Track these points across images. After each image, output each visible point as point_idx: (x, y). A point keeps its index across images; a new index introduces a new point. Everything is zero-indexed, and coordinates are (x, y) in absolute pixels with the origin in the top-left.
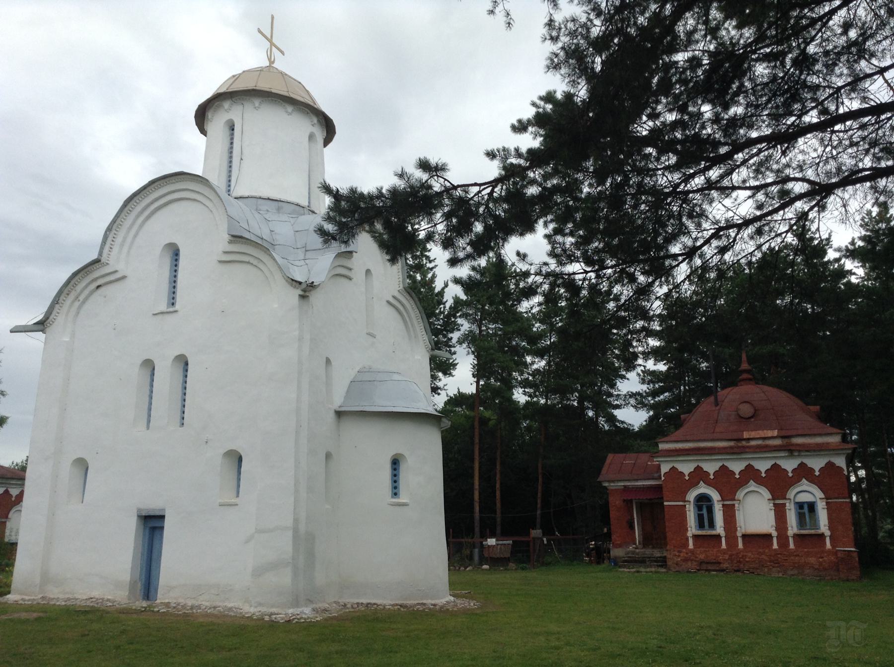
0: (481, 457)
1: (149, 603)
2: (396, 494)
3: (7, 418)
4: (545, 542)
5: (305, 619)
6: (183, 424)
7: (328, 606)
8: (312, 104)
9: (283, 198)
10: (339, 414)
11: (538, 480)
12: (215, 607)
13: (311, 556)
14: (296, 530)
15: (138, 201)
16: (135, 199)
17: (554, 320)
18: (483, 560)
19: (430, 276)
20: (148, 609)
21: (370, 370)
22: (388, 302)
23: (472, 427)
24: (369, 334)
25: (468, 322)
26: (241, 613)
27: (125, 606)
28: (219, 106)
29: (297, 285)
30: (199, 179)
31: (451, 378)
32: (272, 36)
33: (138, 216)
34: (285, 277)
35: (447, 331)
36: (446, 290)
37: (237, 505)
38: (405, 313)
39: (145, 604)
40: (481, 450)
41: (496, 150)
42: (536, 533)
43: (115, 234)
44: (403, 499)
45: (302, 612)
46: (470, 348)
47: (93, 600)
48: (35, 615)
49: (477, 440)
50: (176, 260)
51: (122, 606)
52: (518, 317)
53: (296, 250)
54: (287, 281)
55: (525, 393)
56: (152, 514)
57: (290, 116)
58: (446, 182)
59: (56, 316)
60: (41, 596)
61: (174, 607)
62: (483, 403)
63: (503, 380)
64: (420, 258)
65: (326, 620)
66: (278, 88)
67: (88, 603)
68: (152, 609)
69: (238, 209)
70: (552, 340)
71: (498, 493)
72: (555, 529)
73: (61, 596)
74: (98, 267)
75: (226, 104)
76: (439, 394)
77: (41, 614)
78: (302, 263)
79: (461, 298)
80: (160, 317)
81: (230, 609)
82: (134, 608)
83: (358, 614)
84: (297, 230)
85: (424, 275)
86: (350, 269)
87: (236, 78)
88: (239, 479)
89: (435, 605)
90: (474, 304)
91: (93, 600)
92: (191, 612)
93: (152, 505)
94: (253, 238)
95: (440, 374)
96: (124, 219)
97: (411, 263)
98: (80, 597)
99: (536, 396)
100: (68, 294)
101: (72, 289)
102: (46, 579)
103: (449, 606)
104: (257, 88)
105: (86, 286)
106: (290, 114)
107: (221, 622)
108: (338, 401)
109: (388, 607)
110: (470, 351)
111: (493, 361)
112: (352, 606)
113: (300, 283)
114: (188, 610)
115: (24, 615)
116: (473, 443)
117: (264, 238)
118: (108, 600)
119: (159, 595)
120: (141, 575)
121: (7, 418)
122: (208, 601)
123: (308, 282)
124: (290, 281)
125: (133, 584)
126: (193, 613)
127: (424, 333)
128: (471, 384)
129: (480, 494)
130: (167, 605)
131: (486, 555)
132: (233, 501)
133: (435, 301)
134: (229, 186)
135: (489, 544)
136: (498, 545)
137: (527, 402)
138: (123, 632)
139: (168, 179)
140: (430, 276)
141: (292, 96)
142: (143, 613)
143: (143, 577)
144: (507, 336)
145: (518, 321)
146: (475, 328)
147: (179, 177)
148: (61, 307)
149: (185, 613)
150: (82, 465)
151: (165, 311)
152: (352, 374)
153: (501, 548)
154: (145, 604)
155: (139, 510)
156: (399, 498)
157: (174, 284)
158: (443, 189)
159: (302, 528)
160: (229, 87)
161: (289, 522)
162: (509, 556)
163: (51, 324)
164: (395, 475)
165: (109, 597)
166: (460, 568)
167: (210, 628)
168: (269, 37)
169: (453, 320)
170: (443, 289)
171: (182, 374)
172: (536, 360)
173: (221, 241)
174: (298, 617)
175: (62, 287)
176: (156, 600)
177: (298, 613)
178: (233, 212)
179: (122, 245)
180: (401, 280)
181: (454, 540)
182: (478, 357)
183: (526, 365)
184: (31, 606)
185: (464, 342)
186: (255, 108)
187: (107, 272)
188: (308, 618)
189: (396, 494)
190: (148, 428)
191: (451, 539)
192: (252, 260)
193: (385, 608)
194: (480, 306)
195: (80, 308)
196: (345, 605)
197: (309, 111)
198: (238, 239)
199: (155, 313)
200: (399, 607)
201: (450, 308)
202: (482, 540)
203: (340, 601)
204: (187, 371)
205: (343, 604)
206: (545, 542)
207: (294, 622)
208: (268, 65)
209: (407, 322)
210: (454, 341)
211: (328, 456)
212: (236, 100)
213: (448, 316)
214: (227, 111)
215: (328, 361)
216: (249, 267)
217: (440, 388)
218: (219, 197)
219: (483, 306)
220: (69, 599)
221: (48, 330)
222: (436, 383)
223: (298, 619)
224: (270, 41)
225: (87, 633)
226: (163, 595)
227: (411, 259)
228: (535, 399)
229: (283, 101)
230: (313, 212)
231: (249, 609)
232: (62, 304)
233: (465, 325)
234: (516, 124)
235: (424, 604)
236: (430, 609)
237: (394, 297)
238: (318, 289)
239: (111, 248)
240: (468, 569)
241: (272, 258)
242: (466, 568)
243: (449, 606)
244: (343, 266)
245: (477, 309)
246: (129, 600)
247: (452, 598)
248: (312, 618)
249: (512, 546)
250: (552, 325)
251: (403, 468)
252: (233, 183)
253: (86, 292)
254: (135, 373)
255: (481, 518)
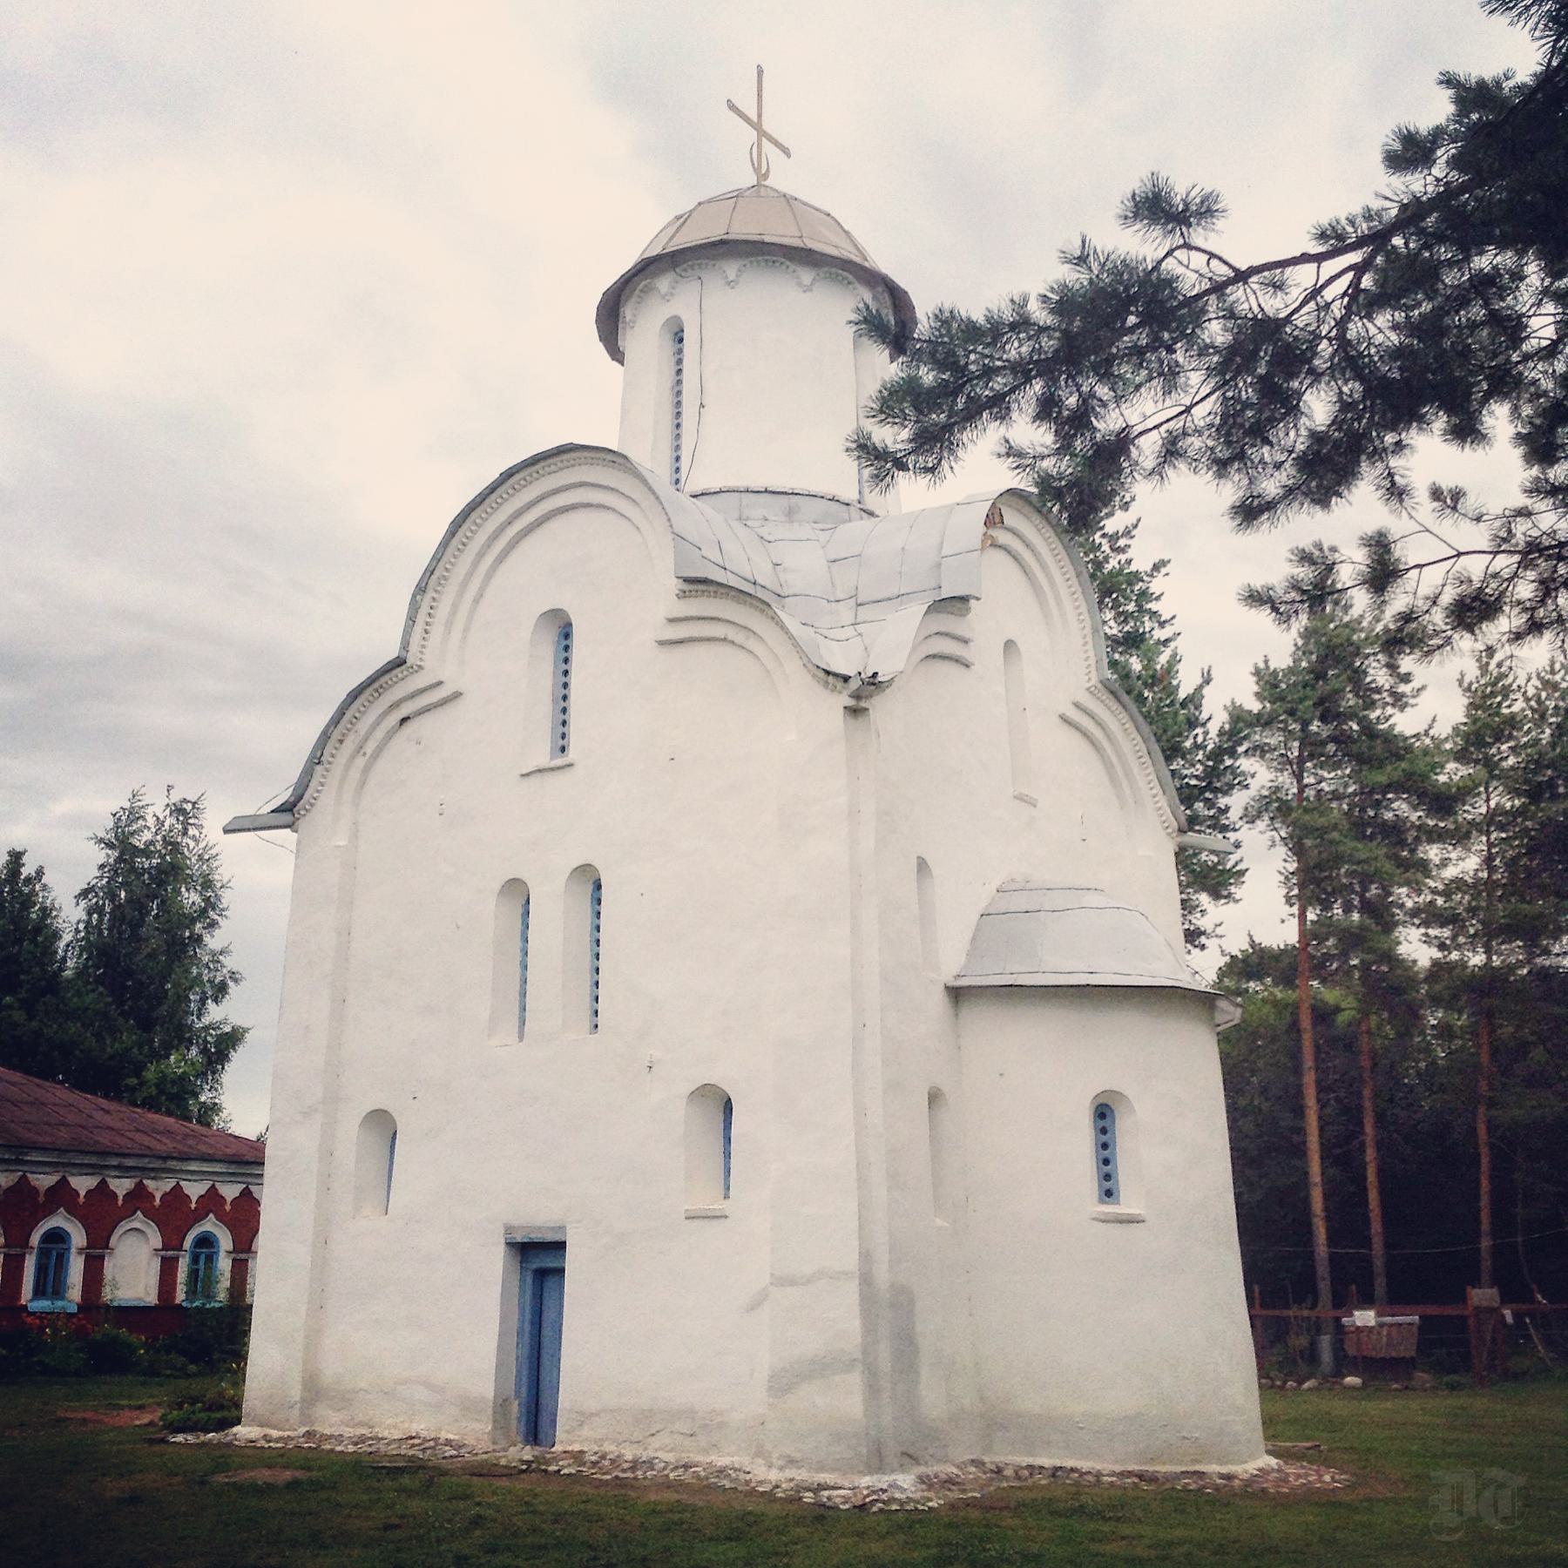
0: (1322, 1105)
1: (538, 1450)
2: (1109, 1193)
3: (246, 1030)
4: (1509, 1319)
5: (901, 1503)
6: (597, 1026)
7: (955, 1471)
8: (858, 260)
9: (799, 486)
10: (957, 994)
11: (1479, 1161)
12: (686, 1467)
13: (906, 1345)
14: (866, 1280)
15: (478, 521)
16: (474, 515)
17: (1494, 751)
18: (1344, 1364)
19: (1163, 659)
20: (534, 1465)
21: (1026, 888)
22: (1065, 719)
23: (1294, 1027)
24: (1019, 798)
25: (1269, 768)
26: (747, 1482)
27: (485, 1456)
28: (647, 290)
29: (840, 684)
30: (610, 457)
31: (1231, 904)
32: (760, 116)
33: (481, 555)
34: (809, 666)
35: (1216, 790)
36: (1205, 691)
37: (726, 1217)
38: (1106, 744)
39: (528, 1453)
40: (1321, 1088)
41: (1344, 222)
42: (1482, 1296)
43: (434, 599)
44: (1128, 1204)
45: (893, 1485)
46: (1275, 829)
47: (416, 1441)
48: (288, 1475)
49: (1308, 1062)
50: (567, 648)
51: (478, 1458)
52: (1396, 748)
53: (834, 604)
54: (814, 676)
55: (1427, 939)
56: (537, 1237)
57: (808, 294)
58: (1214, 262)
59: (318, 791)
60: (303, 1430)
61: (594, 1464)
62: (1319, 968)
63: (1367, 907)
64: (1136, 620)
65: (952, 1506)
66: (780, 231)
67: (404, 1450)
68: (543, 1467)
69: (700, 521)
70: (1493, 804)
71: (1373, 1196)
72: (1534, 1286)
73: (348, 1432)
74: (400, 675)
75: (664, 283)
76: (1203, 947)
77: (299, 1474)
78: (849, 632)
79: (1247, 707)
80: (533, 780)
81: (721, 1471)
82: (503, 1462)
83: (1032, 1495)
84: (832, 558)
85: (1149, 661)
86: (966, 642)
87: (682, 220)
88: (727, 1155)
89: (1229, 1477)
90: (1282, 721)
91: (416, 1441)
92: (629, 1475)
93: (538, 1218)
94: (733, 581)
95: (1204, 899)
96: (452, 564)
97: (1115, 631)
98: (386, 1434)
99: (1459, 947)
100: (341, 741)
101: (348, 730)
102: (314, 1391)
103: (1267, 1481)
104: (731, 237)
105: (377, 723)
106: (808, 289)
107: (701, 1504)
108: (952, 964)
109: (1110, 1479)
110: (1278, 839)
111: (1338, 860)
112: (1016, 1472)
113: (846, 679)
114: (624, 1471)
115: (263, 1476)
116: (1297, 1070)
117: (760, 581)
118: (448, 1443)
119: (560, 1434)
120: (518, 1384)
121: (246, 1030)
122: (671, 1451)
123: (863, 676)
124: (822, 674)
125: (501, 1405)
126: (635, 1478)
127: (1157, 790)
128: (1283, 921)
129: (1326, 1197)
130: (578, 1456)
131: (1351, 1351)
132: (719, 1206)
133: (1181, 718)
134: (678, 470)
135: (1359, 1324)
136: (1381, 1325)
137: (1435, 963)
138: (477, 1521)
139: (542, 464)
140: (1163, 659)
141: (811, 244)
142: (523, 1476)
143: (524, 1390)
144: (1372, 796)
145: (1400, 758)
146: (1286, 780)
147: (565, 457)
148: (327, 770)
149: (617, 1477)
150: (382, 1125)
151: (547, 766)
152: (982, 897)
153: (1389, 1335)
154: (528, 1453)
155: (509, 1229)
156: (1118, 1203)
157: (563, 704)
158: (1206, 285)
159: (882, 1275)
160: (667, 243)
161: (851, 1262)
162: (1413, 1354)
163: (307, 810)
164: (1105, 1146)
165: (451, 1436)
166: (1285, 1383)
167: (676, 1517)
168: (754, 117)
169: (1228, 762)
170: (1200, 688)
171: (589, 910)
172: (1453, 855)
173: (662, 596)
174: (884, 1497)
175: (328, 726)
176: (553, 1446)
177: (885, 1487)
178: (684, 525)
179: (449, 624)
180: (1092, 661)
181: (1264, 1312)
182: (1298, 850)
183: (1424, 867)
184: (282, 1453)
185: (1259, 816)
186: (729, 284)
187: (422, 686)
188: (910, 1500)
189: (1109, 1193)
190: (521, 1037)
191: (1258, 1311)
192: (731, 633)
193: (1098, 1481)
194: (1295, 726)
195: (367, 770)
196: (999, 1471)
197: (851, 277)
198: (701, 587)
199: (524, 772)
200: (1136, 1480)
201: (1221, 733)
202: (1338, 1313)
203: (986, 1459)
204: (599, 902)
205: (993, 1467)
206: (1509, 1319)
207: (875, 1509)
208: (755, 183)
209: (1112, 766)
210: (1234, 815)
211: (934, 1098)
212: (685, 270)
213: (1217, 754)
214: (666, 298)
215: (922, 865)
216: (728, 650)
217: (1203, 933)
218: (654, 493)
219: (1305, 724)
220: (362, 1439)
221: (301, 824)
222: (1194, 921)
223: (884, 1502)
224: (757, 126)
225: (396, 1521)
226: (568, 1432)
227: (1112, 623)
228: (1455, 956)
229: (790, 260)
230: (871, 514)
231: (768, 1474)
232: (330, 763)
233: (1260, 775)
234: (1397, 146)
235: (1201, 1474)
236: (1217, 1488)
237: (1077, 705)
238: (888, 691)
239: (426, 632)
240: (1306, 1385)
241: (777, 624)
242: (1300, 1383)
243: (1267, 1481)
244: (947, 635)
245: (1290, 734)
246: (494, 1443)
247: (1273, 1462)
248: (918, 1502)
249: (1420, 1328)
250: (1490, 764)
251: (1123, 1127)
252: (685, 464)
253: (379, 734)
254: (489, 913)
255: (1333, 1259)
